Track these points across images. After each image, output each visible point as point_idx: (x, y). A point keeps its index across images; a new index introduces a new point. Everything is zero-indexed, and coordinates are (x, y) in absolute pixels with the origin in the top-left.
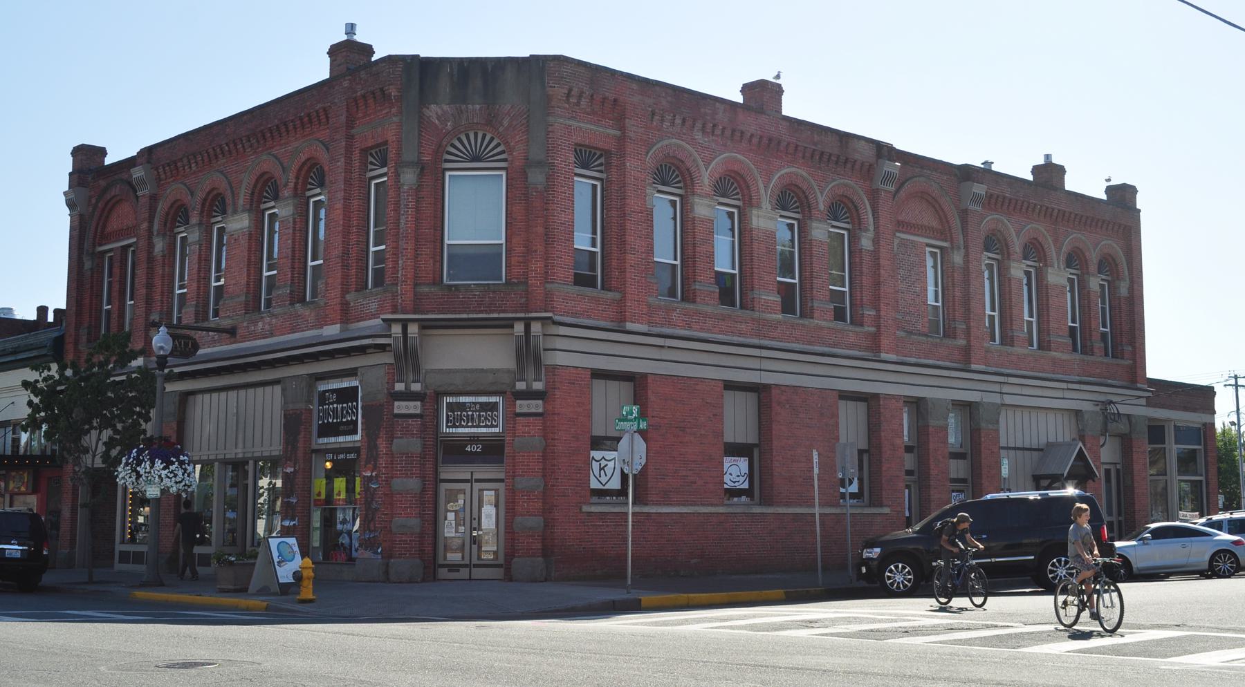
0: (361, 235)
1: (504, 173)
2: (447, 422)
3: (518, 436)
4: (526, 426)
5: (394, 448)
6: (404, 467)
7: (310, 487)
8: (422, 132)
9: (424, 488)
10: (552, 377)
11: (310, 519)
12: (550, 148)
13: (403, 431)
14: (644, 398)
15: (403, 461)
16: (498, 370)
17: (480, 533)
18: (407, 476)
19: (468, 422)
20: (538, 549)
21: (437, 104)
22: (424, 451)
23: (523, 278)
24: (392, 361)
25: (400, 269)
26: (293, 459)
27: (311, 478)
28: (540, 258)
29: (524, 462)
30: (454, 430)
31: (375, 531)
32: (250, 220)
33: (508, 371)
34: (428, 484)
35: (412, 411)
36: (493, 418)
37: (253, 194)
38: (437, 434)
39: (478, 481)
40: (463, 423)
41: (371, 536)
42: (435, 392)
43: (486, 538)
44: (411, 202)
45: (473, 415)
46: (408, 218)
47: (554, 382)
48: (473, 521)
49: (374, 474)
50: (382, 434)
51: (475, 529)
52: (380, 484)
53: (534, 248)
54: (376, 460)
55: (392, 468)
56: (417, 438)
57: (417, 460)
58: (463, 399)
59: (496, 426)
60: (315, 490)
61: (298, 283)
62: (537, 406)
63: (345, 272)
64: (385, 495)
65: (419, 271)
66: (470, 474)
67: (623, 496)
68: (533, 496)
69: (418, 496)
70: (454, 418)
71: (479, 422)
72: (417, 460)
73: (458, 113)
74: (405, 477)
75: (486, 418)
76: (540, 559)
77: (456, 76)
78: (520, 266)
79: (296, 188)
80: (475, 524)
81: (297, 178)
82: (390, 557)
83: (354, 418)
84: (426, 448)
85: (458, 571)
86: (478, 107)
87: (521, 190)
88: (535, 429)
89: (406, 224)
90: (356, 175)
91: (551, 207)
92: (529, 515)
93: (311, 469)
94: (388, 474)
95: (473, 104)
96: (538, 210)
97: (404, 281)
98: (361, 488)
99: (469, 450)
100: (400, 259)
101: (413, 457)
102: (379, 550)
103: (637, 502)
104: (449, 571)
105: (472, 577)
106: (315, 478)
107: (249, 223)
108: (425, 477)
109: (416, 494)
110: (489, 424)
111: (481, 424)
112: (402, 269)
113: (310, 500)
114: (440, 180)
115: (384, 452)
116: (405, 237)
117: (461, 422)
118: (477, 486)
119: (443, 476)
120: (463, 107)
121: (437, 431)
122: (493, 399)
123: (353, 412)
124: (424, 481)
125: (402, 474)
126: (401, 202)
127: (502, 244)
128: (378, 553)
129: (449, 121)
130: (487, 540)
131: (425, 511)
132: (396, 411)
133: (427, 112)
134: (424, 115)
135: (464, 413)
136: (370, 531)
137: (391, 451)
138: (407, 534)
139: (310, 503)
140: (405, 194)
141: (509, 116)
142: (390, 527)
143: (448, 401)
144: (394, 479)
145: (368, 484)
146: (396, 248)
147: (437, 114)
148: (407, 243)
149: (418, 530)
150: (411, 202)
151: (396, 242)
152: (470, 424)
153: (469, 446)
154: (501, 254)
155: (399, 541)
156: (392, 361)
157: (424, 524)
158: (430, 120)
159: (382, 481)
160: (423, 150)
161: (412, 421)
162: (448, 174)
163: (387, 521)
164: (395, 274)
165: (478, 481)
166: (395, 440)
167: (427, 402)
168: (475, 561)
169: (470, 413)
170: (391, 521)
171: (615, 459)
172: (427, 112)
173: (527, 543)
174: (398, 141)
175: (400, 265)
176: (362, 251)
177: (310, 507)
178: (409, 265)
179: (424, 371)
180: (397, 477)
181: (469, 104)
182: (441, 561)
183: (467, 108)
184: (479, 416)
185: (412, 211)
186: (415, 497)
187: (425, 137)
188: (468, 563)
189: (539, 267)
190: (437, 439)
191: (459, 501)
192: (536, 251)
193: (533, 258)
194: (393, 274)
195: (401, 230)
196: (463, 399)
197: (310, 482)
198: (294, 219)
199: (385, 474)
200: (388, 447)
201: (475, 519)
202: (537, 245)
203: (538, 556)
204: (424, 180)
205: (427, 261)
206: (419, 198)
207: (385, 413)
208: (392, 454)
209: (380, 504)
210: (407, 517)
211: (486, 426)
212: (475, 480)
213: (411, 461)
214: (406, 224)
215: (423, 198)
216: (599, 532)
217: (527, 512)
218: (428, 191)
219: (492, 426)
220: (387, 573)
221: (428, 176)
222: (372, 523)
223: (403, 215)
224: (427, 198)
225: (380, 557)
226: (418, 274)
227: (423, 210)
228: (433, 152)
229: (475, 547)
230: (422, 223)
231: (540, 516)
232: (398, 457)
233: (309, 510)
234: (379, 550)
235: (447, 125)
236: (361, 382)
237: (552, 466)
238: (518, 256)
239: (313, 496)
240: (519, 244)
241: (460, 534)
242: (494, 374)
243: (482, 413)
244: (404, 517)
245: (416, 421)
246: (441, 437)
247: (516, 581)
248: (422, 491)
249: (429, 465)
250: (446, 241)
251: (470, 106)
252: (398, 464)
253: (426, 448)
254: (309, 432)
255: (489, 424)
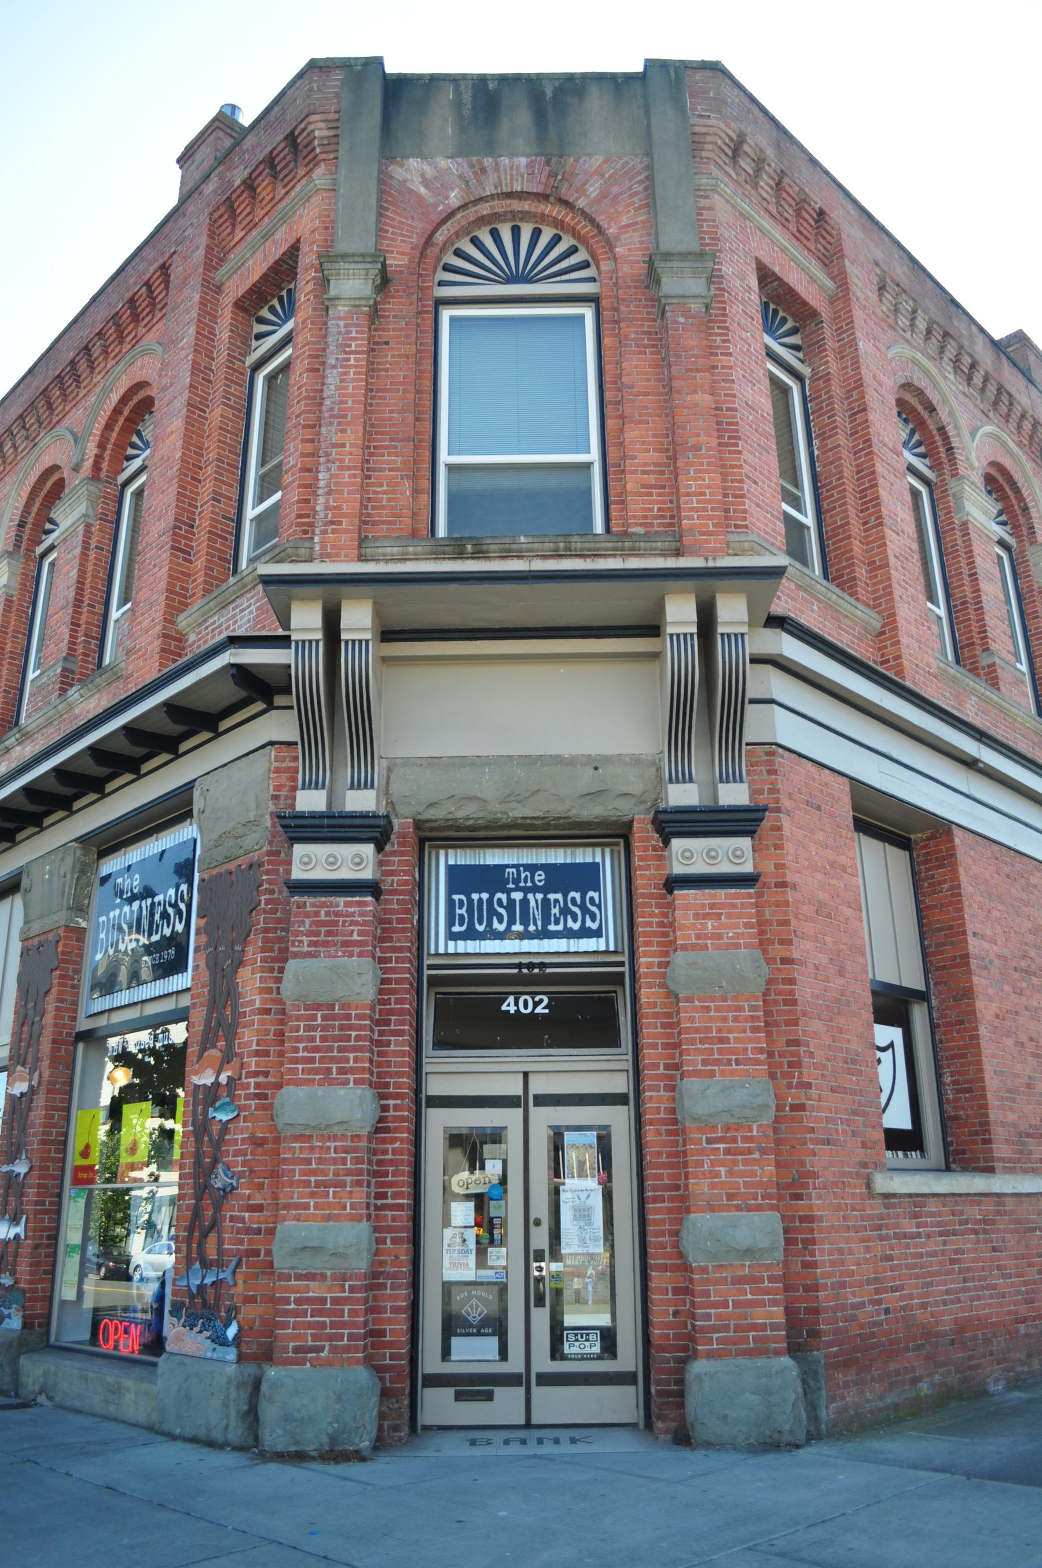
0: (223, 482)
1: (588, 313)
2: (450, 922)
3: (684, 948)
4: (706, 916)
5: (288, 988)
6: (316, 1049)
7: (66, 1135)
8: (387, 209)
9: (382, 1120)
10: (765, 776)
11: (58, 1221)
12: (707, 241)
13: (318, 934)
14: (946, 886)
15: (313, 1029)
16: (607, 759)
17: (555, 1267)
18: (328, 1080)
19: (512, 921)
20: (774, 1327)
21: (423, 157)
22: (382, 1002)
23: (660, 525)
24: (294, 735)
25: (320, 492)
26: (29, 1059)
27: (68, 1110)
28: (709, 464)
29: (708, 1030)
30: (462, 946)
31: (220, 1264)
32: (12, 574)
33: (636, 761)
34: (396, 1108)
35: (345, 874)
36: (585, 911)
37: (21, 525)
38: (420, 958)
39: (543, 1100)
40: (496, 925)
41: (208, 1281)
42: (418, 825)
43: (577, 1284)
44: (356, 339)
45: (525, 902)
46: (346, 373)
47: (772, 791)
48: (532, 1228)
49: (223, 1079)
50: (254, 953)
51: (539, 1256)
52: (240, 1109)
53: (692, 441)
54: (231, 1035)
55: (281, 1054)
56: (361, 955)
57: (360, 1028)
58: (493, 857)
59: (597, 934)
60: (76, 1143)
61: (84, 654)
62: (737, 855)
63: (179, 564)
64: (257, 1143)
65: (374, 508)
66: (520, 1078)
67: (915, 1150)
68: (746, 1140)
69: (364, 1144)
70: (470, 911)
71: (546, 921)
72: (360, 1028)
73: (475, 173)
74: (321, 1083)
75: (565, 911)
76: (786, 1361)
77: (469, 106)
78: (650, 494)
79: (96, 467)
80: (540, 1239)
81: (102, 446)
82: (267, 1356)
83: (180, 928)
84: (391, 992)
85: (489, 1397)
86: (523, 161)
87: (643, 326)
88: (735, 926)
89: (341, 388)
90: (221, 357)
91: (719, 361)
92: (738, 1208)
93: (71, 1084)
94: (266, 1074)
95: (512, 155)
96: (692, 356)
97: (332, 523)
98: (872, 1412)
99: (512, 1009)
100: (322, 468)
101: (348, 1017)
102: (231, 1332)
103: (953, 1166)
104: (459, 1397)
105: (534, 1422)
106: (80, 1108)
107: (8, 580)
108: (387, 1085)
109: (356, 1137)
110: (576, 926)
111: (552, 927)
112: (329, 493)
113: (63, 1169)
114: (427, 312)
115: (257, 1005)
116: (338, 417)
117: (490, 923)
118: (543, 1118)
119: (435, 1087)
120: (488, 161)
121: (420, 949)
122: (583, 856)
123: (179, 912)
124: (382, 1096)
125: (310, 1071)
126: (330, 339)
127: (588, 466)
128: (223, 1342)
129: (453, 189)
130: (578, 1293)
131: (384, 1196)
132: (298, 873)
133: (397, 172)
134: (391, 177)
135: (499, 895)
136: (206, 1265)
137: (280, 1002)
138: (324, 1277)
139: (62, 1178)
140: (342, 323)
141: (602, 176)
142: (269, 1253)
143: (451, 862)
144: (284, 1090)
145: (205, 1113)
146: (311, 455)
147: (423, 175)
148: (343, 431)
149: (361, 1264)
150: (356, 339)
151: (312, 441)
152: (518, 927)
153: (511, 999)
154: (588, 492)
155: (297, 1301)
156: (294, 735)
157: (380, 1241)
158: (408, 188)
159: (247, 1097)
160: (388, 245)
161: (347, 904)
162: (447, 314)
163: (258, 1231)
164: (308, 516)
165: (543, 1100)
166: (292, 965)
167: (393, 853)
168: (543, 1363)
169: (517, 896)
170: (272, 1232)
171: (891, 1045)
172: (397, 172)
173: (737, 1304)
174: (327, 228)
175: (322, 484)
176: (224, 517)
177: (61, 1186)
178: (347, 484)
179: (384, 763)
180: (298, 1083)
181: (500, 156)
182: (431, 1363)
183: (497, 164)
184: (546, 902)
185: (356, 360)
186: (355, 1150)
187: (393, 219)
188: (521, 1369)
189: (709, 486)
190: (419, 970)
191: (488, 1164)
192: (697, 448)
193: (692, 464)
194: (299, 516)
195: (327, 402)
196: (493, 857)
197: (67, 1119)
198: (88, 526)
199: (256, 1074)
200: (270, 990)
201: (538, 1223)
202: (698, 435)
203: (777, 1353)
204: (387, 306)
205: (396, 484)
206: (375, 343)
207: (266, 886)
208: (283, 1012)
209: (241, 1175)
210: (327, 1218)
211: (568, 934)
212: (536, 1097)
213: (342, 1028)
214: (341, 388)
215: (387, 343)
216: (914, 1256)
217: (731, 1197)
218: (400, 330)
219: (585, 933)
220: (252, 1415)
221: (401, 297)
222: (213, 1236)
223: (334, 367)
224: (397, 343)
225: (231, 1354)
226: (368, 515)
227: (386, 370)
228: (412, 249)
229: (541, 1317)
230: (385, 398)
231: (772, 1208)
232: (298, 1018)
233: (60, 1195)
234: (231, 1332)
235: (447, 197)
236: (201, 829)
237: (789, 1043)
238: (644, 472)
239: (73, 1159)
240: (643, 443)
241: (492, 1272)
242: (596, 768)
243: (552, 896)
244: (313, 1218)
245: (360, 904)
246: (431, 967)
247: (709, 1445)
248: (377, 1130)
249: (399, 1045)
250: (445, 458)
251: (505, 161)
252: (299, 1039)
253: (391, 992)
254: (73, 987)
255: (576, 926)
